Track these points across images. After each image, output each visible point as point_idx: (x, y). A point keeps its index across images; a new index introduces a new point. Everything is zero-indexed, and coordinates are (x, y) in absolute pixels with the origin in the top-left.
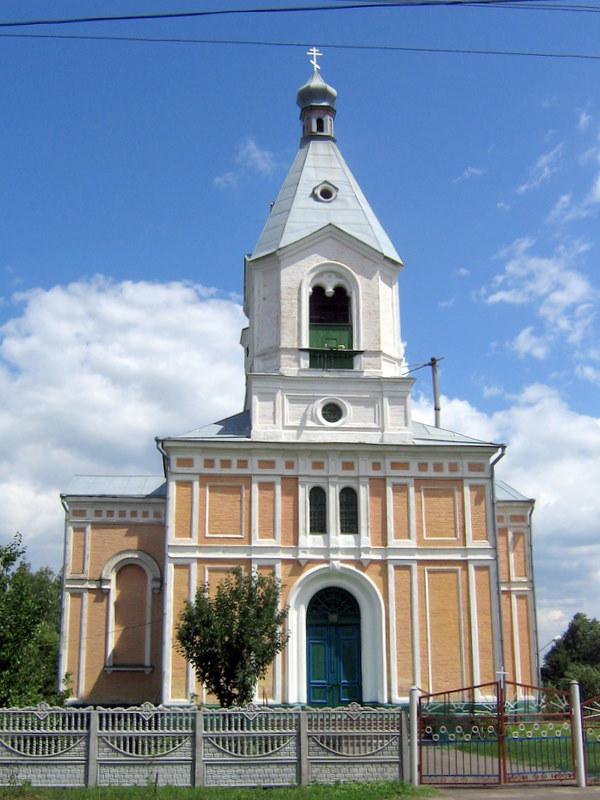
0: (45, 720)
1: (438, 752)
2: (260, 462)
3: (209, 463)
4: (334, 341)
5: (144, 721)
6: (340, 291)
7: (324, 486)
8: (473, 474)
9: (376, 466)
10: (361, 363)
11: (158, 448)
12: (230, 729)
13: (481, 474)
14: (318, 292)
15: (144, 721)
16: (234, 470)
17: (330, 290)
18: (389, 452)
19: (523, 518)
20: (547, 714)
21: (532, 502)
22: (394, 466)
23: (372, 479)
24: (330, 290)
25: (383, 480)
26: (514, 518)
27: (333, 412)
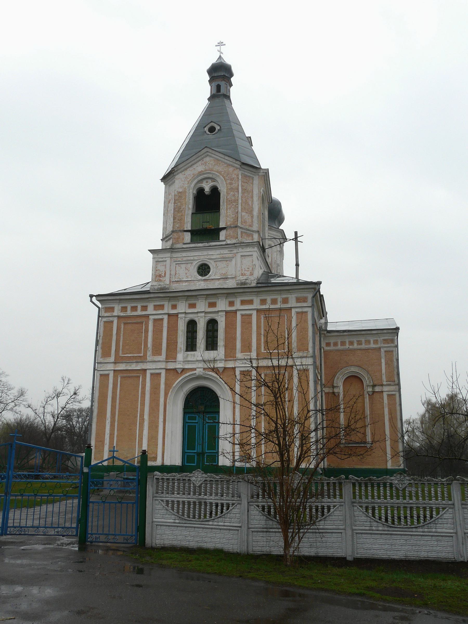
0: (200, 487)
1: (156, 515)
2: (155, 306)
3: (124, 309)
4: (206, 221)
5: (195, 487)
6: (215, 191)
7: (196, 319)
8: (299, 305)
9: (231, 304)
10: (222, 235)
11: (91, 301)
12: (379, 498)
13: (305, 304)
14: (201, 191)
15: (397, 489)
16: (139, 312)
17: (207, 189)
18: (238, 293)
19: (392, 341)
20: (122, 488)
21: (398, 329)
22: (243, 302)
23: (227, 312)
24: (207, 189)
25: (235, 312)
26: (385, 341)
27: (204, 269)
